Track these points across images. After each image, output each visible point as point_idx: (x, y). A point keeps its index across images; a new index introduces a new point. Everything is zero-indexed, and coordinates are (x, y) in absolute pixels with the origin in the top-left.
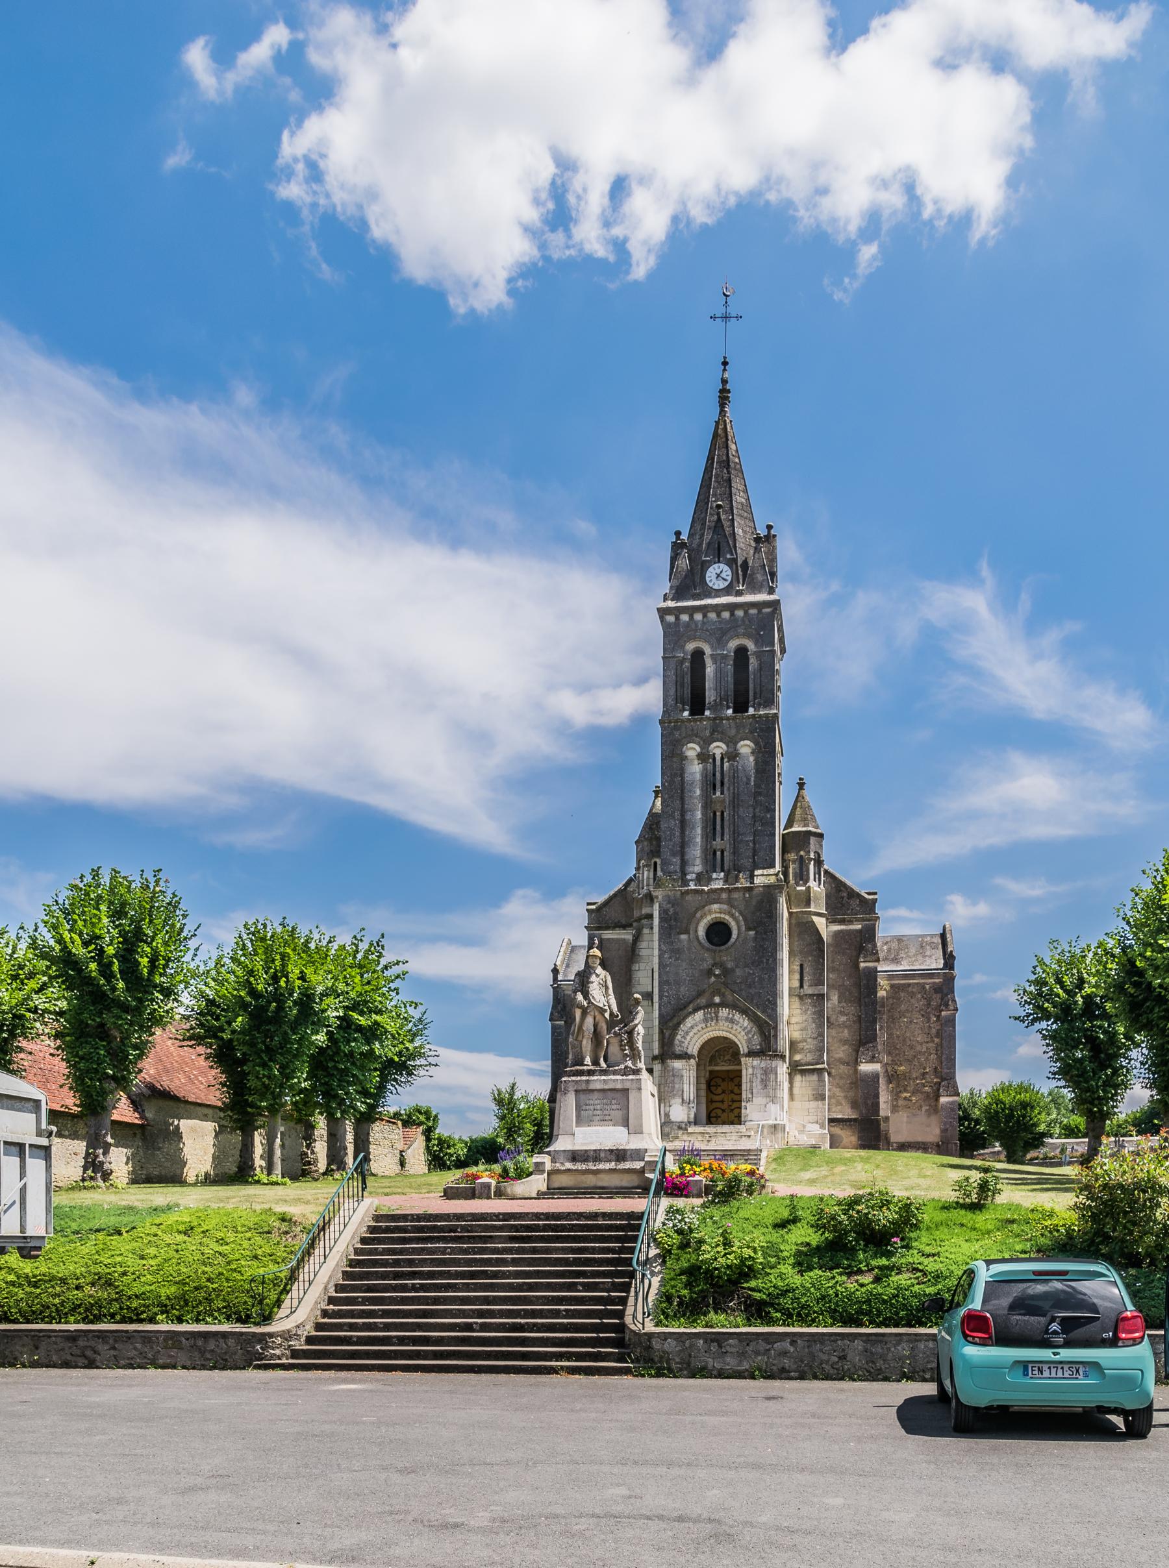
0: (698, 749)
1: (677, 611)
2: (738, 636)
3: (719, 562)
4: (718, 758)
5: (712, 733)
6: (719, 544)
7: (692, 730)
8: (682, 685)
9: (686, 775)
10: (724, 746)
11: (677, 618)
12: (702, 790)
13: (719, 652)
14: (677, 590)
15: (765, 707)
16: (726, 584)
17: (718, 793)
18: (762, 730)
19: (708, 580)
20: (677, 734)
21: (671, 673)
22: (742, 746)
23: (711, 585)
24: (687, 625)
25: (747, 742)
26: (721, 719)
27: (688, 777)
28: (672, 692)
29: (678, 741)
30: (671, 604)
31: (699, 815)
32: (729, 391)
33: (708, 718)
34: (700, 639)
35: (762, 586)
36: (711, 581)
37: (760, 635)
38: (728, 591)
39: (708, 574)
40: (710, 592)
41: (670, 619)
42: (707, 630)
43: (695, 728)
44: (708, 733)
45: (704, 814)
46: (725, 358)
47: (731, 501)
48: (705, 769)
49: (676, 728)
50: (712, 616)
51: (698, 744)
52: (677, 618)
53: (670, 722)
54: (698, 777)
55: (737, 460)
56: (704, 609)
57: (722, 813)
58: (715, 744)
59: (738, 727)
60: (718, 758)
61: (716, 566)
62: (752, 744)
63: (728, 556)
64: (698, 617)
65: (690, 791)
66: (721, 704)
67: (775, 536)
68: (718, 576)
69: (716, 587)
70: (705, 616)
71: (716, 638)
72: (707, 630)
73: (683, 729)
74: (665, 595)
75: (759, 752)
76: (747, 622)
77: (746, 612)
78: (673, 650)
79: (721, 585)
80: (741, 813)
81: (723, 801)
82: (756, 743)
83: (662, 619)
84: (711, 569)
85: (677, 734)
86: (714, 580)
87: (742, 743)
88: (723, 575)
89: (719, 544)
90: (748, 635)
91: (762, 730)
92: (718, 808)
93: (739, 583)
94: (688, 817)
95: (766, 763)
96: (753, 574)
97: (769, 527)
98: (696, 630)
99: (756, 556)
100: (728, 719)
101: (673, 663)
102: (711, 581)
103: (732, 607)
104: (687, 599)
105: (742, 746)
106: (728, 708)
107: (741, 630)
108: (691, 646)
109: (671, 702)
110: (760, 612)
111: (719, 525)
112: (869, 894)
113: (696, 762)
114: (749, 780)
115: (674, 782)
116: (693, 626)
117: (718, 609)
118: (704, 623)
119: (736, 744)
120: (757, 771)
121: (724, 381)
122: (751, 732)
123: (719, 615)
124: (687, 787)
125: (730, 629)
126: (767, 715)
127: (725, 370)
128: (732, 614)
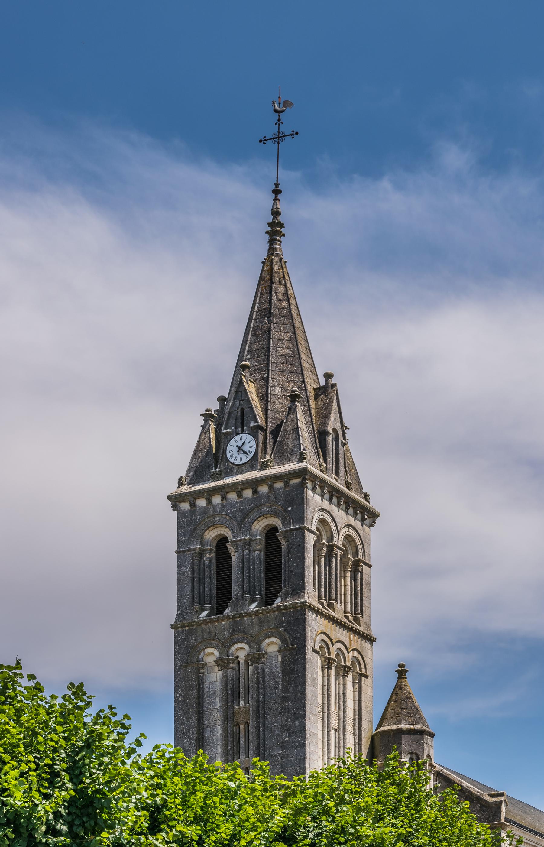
0: (217, 653)
1: (194, 496)
2: (263, 516)
3: (242, 432)
4: (242, 661)
5: (232, 634)
6: (242, 411)
7: (210, 633)
8: (201, 581)
9: (206, 685)
10: (246, 647)
11: (193, 505)
12: (222, 701)
13: (240, 538)
14: (195, 472)
15: (293, 595)
16: (250, 456)
17: (242, 703)
18: (288, 623)
19: (228, 455)
20: (192, 639)
21: (187, 570)
22: (269, 645)
23: (232, 460)
24: (205, 511)
25: (273, 639)
26: (242, 616)
27: (208, 688)
28: (188, 591)
29: (194, 647)
30: (185, 489)
31: (219, 730)
32: (281, 225)
33: (227, 617)
34: (221, 525)
35: (291, 454)
36: (232, 456)
37: (287, 512)
38: (252, 464)
39: (229, 448)
40: (231, 470)
41: (185, 506)
42: (227, 514)
43: (212, 630)
44: (227, 634)
45: (225, 730)
46: (277, 185)
47: (268, 356)
48: (226, 676)
49: (192, 632)
50: (217, 500)
51: (216, 647)
52: (193, 505)
53: (184, 627)
54: (218, 686)
55: (285, 304)
56: (222, 491)
57: (247, 724)
58: (236, 646)
59: (261, 623)
60: (242, 661)
61: (237, 438)
62: (278, 641)
63: (252, 424)
64: (202, 503)
65: (210, 703)
66: (243, 598)
67: (334, 385)
68: (240, 449)
69: (238, 462)
70: (224, 498)
71: (237, 523)
72: (227, 514)
73: (200, 633)
74: (180, 479)
75: (285, 650)
76: (273, 499)
77: (271, 488)
78: (189, 542)
79: (245, 459)
80: (268, 723)
81: (248, 712)
82: (283, 640)
83: (175, 508)
84: (232, 442)
85: (192, 639)
86: (236, 454)
87: (267, 641)
88: (246, 448)
89: (242, 411)
90: (275, 514)
91: (288, 623)
92: (242, 719)
93: (265, 453)
94: (207, 735)
95: (294, 661)
96: (284, 439)
97: (328, 376)
98: (214, 516)
99: (290, 418)
100: (249, 615)
101: (188, 557)
102: (232, 456)
103: (254, 484)
104: (205, 481)
105: (269, 645)
106: (253, 601)
107: (266, 509)
108: (211, 535)
109: (186, 602)
110: (286, 484)
111: (241, 389)
112: (493, 796)
113: (216, 669)
114: (277, 683)
115: (189, 695)
116: (211, 512)
117: (239, 488)
118: (223, 506)
119: (259, 643)
120: (284, 672)
121: (276, 213)
122: (277, 627)
123: (239, 495)
124: (207, 699)
125: (253, 508)
126: (294, 606)
127: (276, 200)
128: (255, 492)
